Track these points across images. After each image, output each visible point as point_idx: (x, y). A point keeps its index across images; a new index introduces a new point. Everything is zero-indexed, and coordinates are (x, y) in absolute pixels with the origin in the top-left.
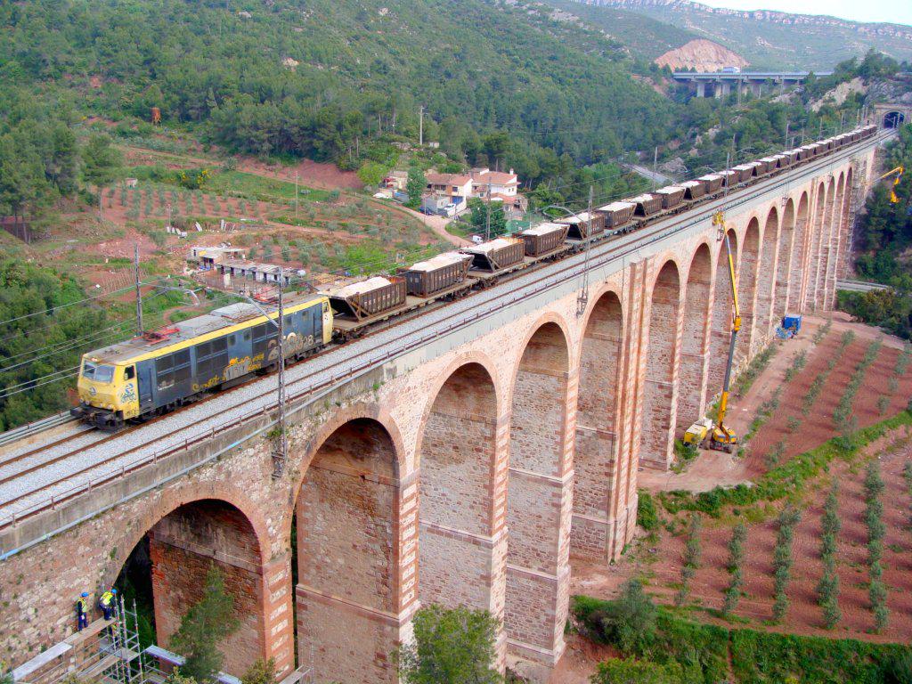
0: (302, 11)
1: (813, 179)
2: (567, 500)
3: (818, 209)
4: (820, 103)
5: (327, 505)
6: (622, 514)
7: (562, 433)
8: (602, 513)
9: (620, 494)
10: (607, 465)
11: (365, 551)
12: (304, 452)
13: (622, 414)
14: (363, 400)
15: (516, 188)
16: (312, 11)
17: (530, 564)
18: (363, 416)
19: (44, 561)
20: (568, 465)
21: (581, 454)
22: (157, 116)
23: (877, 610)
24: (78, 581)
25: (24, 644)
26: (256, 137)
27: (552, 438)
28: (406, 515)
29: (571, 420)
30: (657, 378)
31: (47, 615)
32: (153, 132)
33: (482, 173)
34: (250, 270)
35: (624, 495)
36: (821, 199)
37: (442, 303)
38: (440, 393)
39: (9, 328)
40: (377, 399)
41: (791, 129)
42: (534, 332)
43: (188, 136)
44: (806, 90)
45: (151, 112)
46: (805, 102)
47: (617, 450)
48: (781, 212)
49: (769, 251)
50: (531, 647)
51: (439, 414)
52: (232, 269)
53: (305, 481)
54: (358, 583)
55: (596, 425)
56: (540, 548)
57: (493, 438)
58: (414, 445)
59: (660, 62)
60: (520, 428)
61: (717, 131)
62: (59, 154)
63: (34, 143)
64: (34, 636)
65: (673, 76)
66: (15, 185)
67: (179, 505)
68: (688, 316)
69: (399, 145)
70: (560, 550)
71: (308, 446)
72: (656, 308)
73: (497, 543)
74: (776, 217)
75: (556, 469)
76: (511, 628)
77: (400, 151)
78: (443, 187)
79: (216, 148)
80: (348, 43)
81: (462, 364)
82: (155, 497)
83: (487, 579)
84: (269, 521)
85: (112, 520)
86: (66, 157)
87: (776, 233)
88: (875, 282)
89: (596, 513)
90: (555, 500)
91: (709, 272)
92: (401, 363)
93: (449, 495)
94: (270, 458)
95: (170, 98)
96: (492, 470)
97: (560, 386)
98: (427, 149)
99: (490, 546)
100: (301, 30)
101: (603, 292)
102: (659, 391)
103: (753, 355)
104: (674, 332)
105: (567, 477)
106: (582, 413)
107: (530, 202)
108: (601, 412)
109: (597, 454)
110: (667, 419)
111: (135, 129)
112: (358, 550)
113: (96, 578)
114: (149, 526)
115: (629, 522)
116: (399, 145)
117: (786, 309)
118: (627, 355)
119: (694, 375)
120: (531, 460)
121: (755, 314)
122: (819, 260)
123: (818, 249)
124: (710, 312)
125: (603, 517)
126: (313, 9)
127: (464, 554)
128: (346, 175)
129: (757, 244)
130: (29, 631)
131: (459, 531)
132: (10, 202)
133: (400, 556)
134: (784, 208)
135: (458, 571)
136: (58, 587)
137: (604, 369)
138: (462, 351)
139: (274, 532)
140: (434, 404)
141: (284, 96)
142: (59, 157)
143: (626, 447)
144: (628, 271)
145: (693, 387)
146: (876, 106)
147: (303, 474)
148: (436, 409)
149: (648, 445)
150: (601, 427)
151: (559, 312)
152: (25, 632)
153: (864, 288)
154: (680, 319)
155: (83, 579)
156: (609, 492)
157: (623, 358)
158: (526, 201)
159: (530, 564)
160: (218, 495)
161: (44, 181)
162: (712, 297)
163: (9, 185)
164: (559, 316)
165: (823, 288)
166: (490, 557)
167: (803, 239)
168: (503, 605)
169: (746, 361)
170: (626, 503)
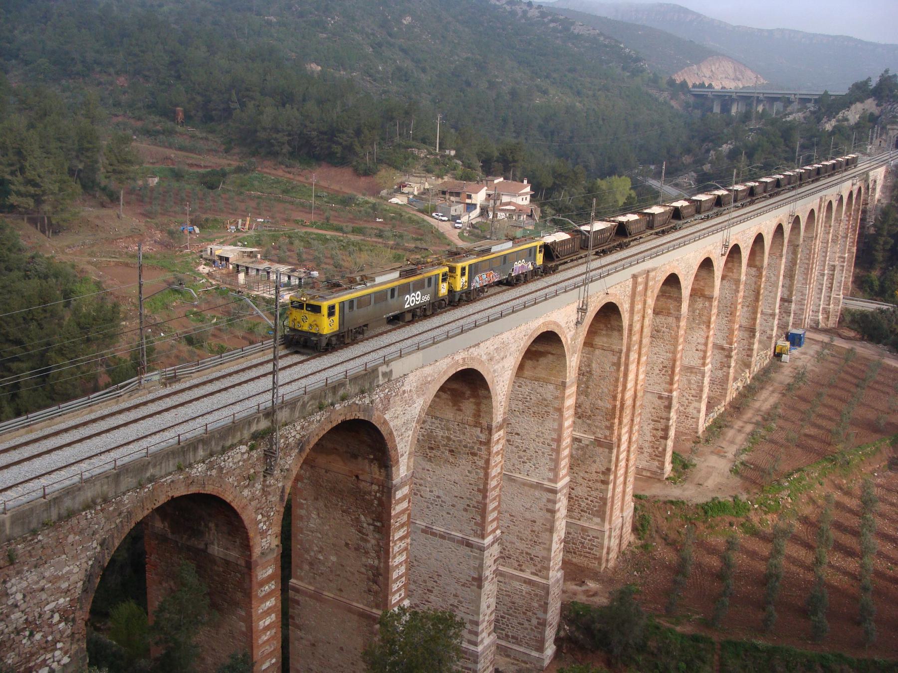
0: (327, 17)
1: (821, 198)
2: (562, 505)
3: (825, 227)
4: (833, 122)
5: (321, 504)
6: (617, 521)
7: (559, 440)
8: (597, 520)
9: (615, 502)
10: (603, 473)
11: (357, 549)
12: (297, 451)
13: (620, 423)
14: (357, 402)
15: (529, 197)
16: (337, 18)
17: (523, 567)
18: (356, 418)
19: (33, 548)
20: (563, 472)
21: (575, 463)
22: (181, 116)
23: (866, 625)
24: (67, 568)
25: (11, 629)
26: (276, 139)
27: (549, 445)
28: (262, 584)
29: (568, 428)
30: (657, 389)
31: (35, 601)
32: (176, 132)
33: (496, 181)
34: (264, 270)
35: (619, 503)
36: (828, 217)
37: (504, 288)
38: (435, 396)
39: (24, 319)
40: (372, 402)
41: (803, 147)
42: (532, 340)
43: (210, 136)
44: (820, 109)
45: (175, 112)
46: (819, 120)
47: (614, 459)
48: (787, 229)
49: (774, 267)
50: (522, 649)
51: (436, 418)
52: (247, 268)
53: (298, 479)
54: (349, 581)
55: (594, 433)
56: (533, 553)
57: (488, 443)
58: (408, 447)
59: (678, 78)
60: (518, 434)
61: (731, 147)
62: (82, 150)
63: (59, 140)
64: (21, 621)
65: (690, 91)
66: (38, 180)
67: (170, 498)
68: (690, 328)
69: (416, 151)
70: (553, 554)
71: (301, 445)
72: (658, 320)
73: (489, 547)
74: (782, 234)
75: (551, 475)
76: (504, 630)
77: (416, 158)
78: (458, 194)
79: (236, 150)
80: (371, 50)
81: (459, 370)
82: (146, 490)
83: (479, 581)
84: (260, 517)
85: (102, 510)
86: (89, 154)
87: (782, 250)
88: (882, 301)
89: (591, 519)
90: (550, 506)
91: (713, 287)
92: (398, 368)
93: (444, 497)
94: (262, 455)
95: (193, 99)
96: (487, 475)
97: (558, 393)
98: (443, 156)
99: (482, 549)
100: (325, 35)
101: (604, 302)
102: (659, 402)
103: (756, 369)
104: (675, 345)
105: (563, 482)
106: (580, 421)
107: (542, 211)
108: (600, 421)
109: (594, 462)
110: (666, 429)
111: (158, 128)
112: (350, 549)
113: (85, 565)
114: (140, 518)
115: (624, 530)
116: (416, 151)
117: (791, 324)
118: (627, 366)
119: (695, 387)
120: (527, 465)
121: (758, 327)
122: (825, 278)
123: (824, 266)
124: (712, 326)
125: (597, 524)
126: (338, 16)
127: (457, 555)
128: (363, 179)
129: (762, 260)
130: (17, 617)
131: (453, 533)
132: (32, 196)
133: (391, 555)
134: (790, 225)
135: (450, 572)
136: (47, 574)
137: (604, 379)
138: (459, 357)
139: (265, 527)
140: (430, 406)
141: (304, 100)
142: (82, 154)
143: (623, 456)
144: (630, 283)
145: (693, 398)
146: (888, 127)
147: (295, 473)
148: (432, 411)
149: (646, 454)
150: (600, 436)
151: (558, 321)
152: (12, 616)
153: (869, 306)
154: (681, 332)
155: (72, 567)
156: (604, 500)
157: (622, 368)
158: (539, 210)
159: (523, 567)
160: (209, 490)
161: (66, 177)
162: (714, 311)
163: (33, 180)
164: (558, 326)
165: (829, 305)
166: (483, 560)
167: (809, 256)
168: (493, 607)
169: (748, 375)
170: (622, 510)
